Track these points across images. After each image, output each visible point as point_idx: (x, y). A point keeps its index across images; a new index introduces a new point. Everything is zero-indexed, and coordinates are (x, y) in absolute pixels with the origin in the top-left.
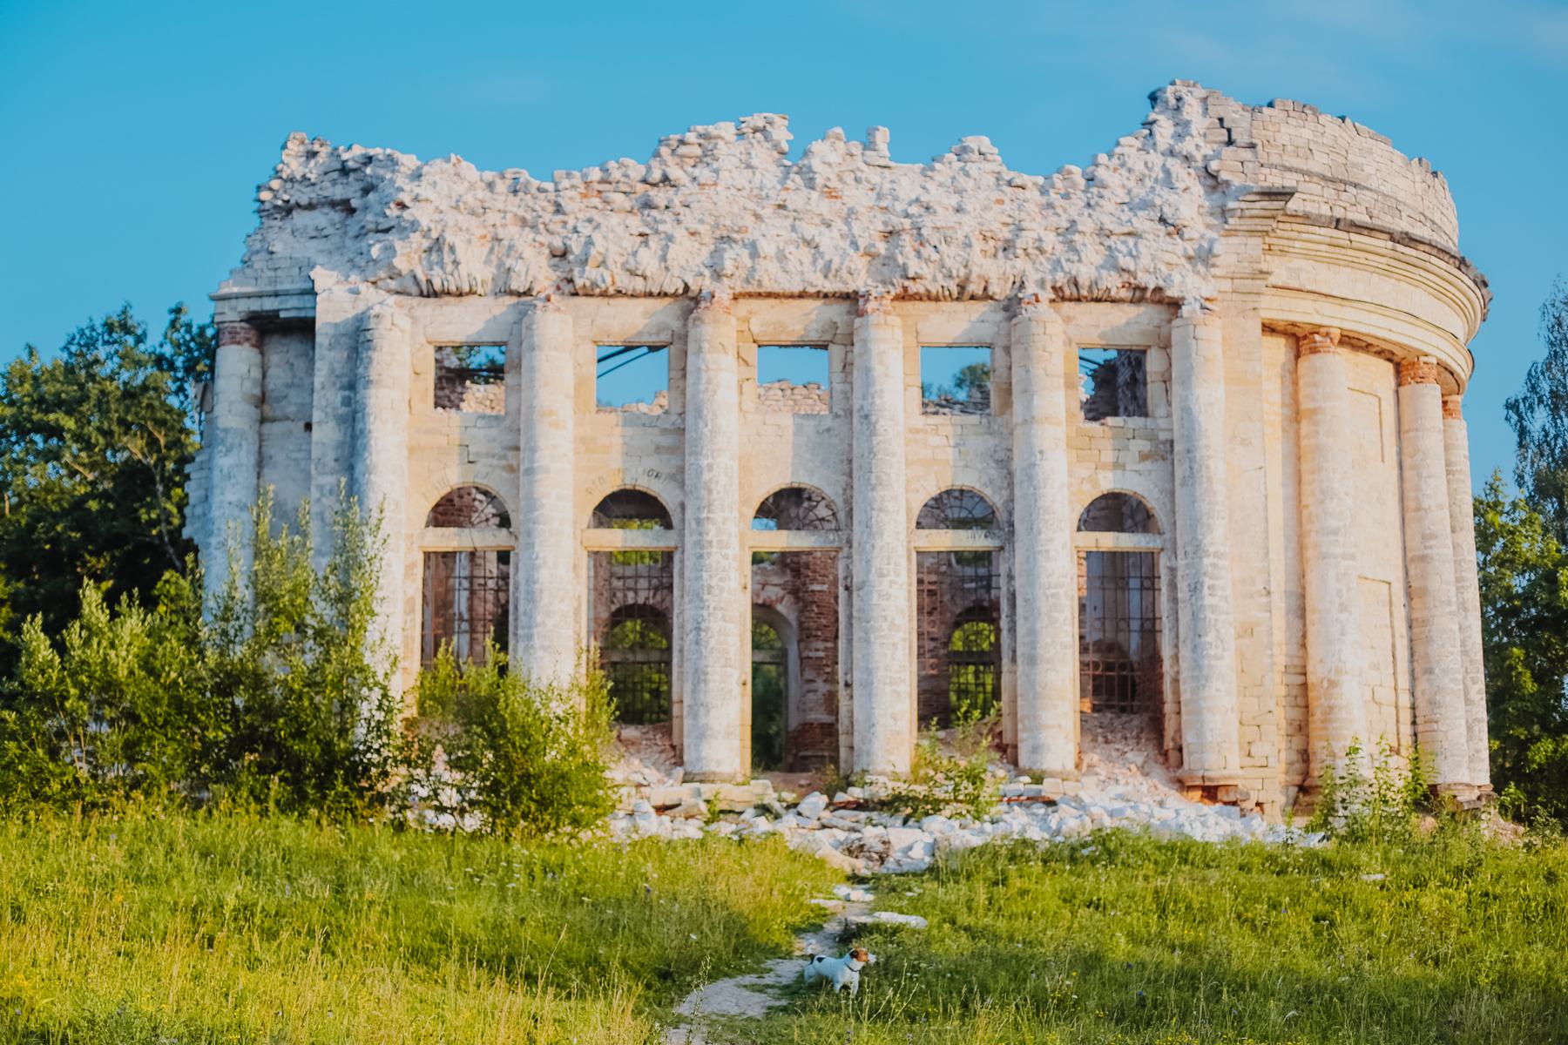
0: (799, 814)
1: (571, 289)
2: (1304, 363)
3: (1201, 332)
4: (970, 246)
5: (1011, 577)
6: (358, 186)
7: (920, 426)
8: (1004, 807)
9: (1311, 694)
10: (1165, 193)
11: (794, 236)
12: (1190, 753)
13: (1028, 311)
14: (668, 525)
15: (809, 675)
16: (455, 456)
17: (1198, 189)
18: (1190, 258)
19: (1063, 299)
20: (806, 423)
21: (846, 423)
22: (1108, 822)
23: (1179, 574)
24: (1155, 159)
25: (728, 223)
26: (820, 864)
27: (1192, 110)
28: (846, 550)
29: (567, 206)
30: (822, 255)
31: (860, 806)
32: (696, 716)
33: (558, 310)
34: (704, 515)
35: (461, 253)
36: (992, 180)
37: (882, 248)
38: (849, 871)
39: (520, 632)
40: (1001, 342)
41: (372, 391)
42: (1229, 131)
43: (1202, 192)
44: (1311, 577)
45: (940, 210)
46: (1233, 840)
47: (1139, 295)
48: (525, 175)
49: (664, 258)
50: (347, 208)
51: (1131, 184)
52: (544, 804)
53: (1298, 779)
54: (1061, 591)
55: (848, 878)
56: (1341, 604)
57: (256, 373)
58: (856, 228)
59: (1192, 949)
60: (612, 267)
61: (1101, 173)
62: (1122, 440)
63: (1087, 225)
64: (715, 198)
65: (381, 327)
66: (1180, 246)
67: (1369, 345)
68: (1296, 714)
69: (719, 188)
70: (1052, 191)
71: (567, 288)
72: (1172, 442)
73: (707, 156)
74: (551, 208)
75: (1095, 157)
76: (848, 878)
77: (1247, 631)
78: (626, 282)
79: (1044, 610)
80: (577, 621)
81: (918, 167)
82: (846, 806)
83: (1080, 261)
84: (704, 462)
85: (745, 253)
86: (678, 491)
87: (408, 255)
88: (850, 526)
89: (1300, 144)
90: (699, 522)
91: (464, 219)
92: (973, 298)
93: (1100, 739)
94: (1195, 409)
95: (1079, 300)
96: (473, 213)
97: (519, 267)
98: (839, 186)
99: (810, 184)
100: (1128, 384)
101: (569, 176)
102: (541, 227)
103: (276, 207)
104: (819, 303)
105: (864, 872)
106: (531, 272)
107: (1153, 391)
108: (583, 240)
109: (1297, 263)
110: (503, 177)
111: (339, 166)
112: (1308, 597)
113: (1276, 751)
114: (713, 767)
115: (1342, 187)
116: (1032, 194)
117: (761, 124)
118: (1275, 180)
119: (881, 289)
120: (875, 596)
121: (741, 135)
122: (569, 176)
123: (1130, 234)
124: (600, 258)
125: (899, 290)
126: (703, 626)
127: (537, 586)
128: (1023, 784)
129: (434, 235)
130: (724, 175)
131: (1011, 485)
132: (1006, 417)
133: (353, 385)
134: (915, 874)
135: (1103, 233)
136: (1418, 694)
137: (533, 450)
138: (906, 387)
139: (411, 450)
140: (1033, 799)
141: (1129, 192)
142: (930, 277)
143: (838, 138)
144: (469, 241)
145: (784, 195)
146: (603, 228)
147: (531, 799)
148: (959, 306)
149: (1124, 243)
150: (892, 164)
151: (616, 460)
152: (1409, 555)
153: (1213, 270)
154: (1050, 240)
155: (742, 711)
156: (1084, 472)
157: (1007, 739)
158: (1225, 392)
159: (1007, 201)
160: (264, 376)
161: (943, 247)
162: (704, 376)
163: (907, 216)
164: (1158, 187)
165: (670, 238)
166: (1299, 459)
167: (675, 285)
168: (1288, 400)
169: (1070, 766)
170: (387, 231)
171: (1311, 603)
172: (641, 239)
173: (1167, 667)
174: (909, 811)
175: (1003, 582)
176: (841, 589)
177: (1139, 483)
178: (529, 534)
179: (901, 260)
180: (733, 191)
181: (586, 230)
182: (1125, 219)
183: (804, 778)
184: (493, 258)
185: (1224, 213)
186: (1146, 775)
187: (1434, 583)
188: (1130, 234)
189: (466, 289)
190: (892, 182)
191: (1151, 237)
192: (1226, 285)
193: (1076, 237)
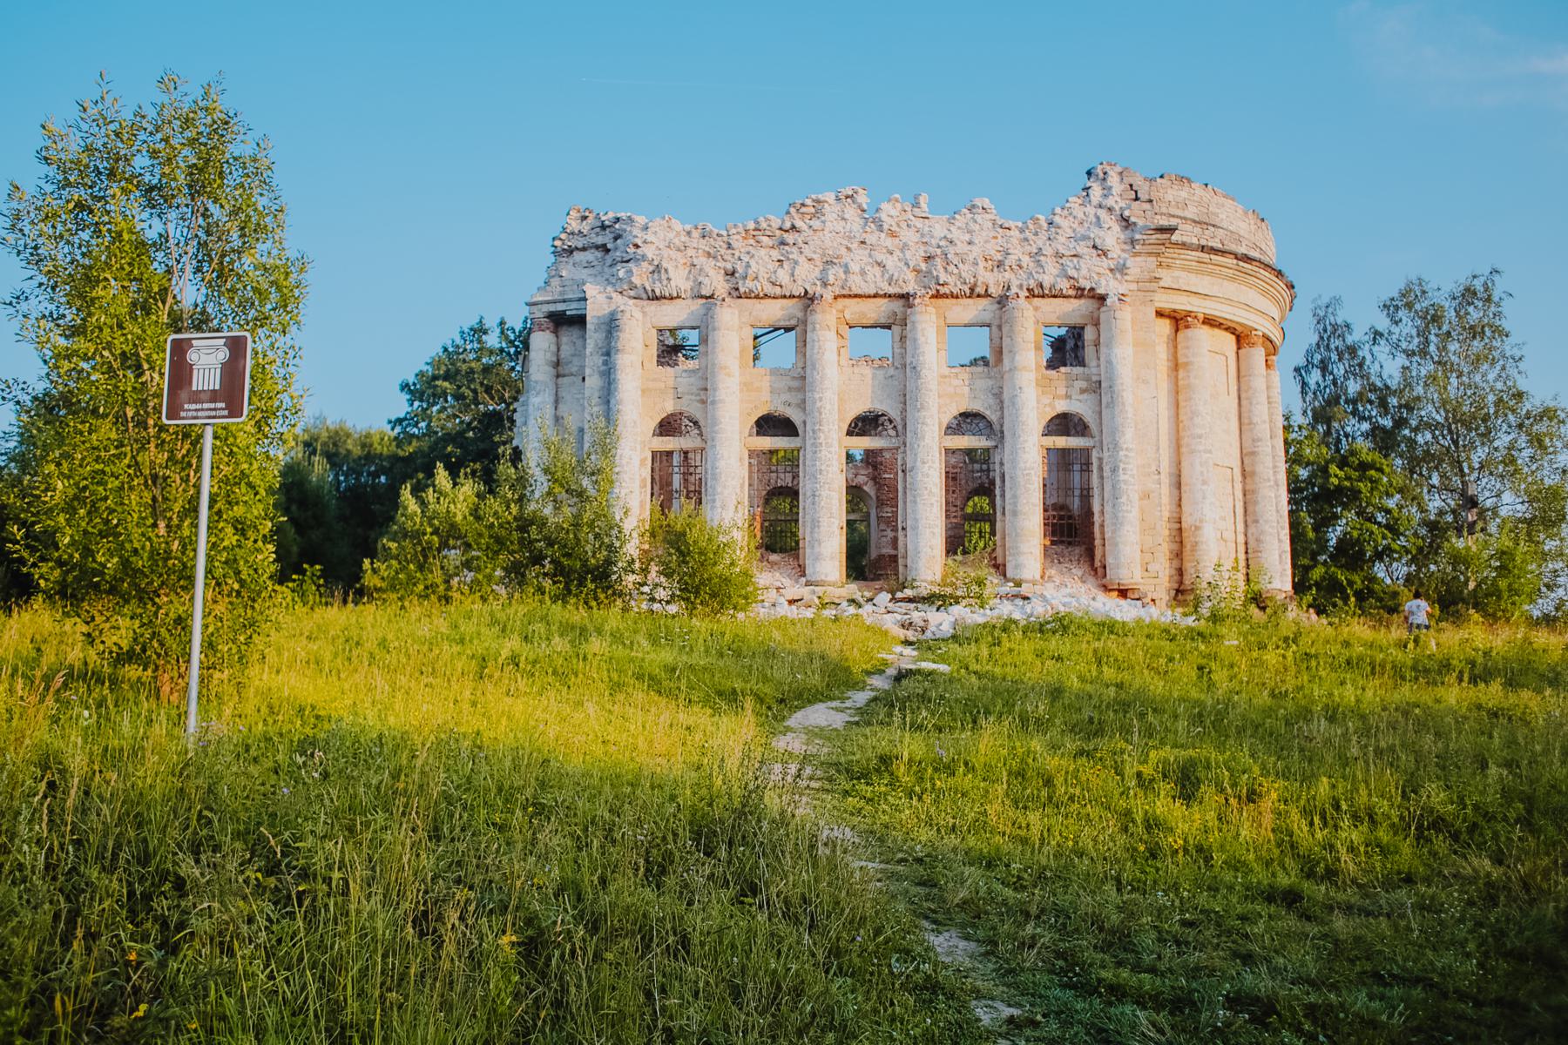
5: (1002, 464)
10: (1096, 230)
13: (1012, 304)
17: (1116, 228)
21: (902, 371)
24: (1090, 210)
27: (1113, 180)
31: (910, 600)
35: (671, 275)
37: (923, 266)
40: (996, 322)
47: (1080, 293)
50: (605, 249)
53: (1176, 586)
57: (554, 348)
58: (908, 254)
59: (1120, 686)
61: (1057, 219)
62: (1071, 379)
63: (1048, 251)
66: (1105, 263)
68: (1175, 547)
71: (735, 294)
77: (1146, 496)
84: (817, 396)
88: (905, 434)
89: (1177, 201)
91: (673, 253)
97: (706, 281)
105: (912, 639)
107: (1089, 351)
109: (1177, 273)
116: (1015, 233)
121: (838, 199)
131: (1002, 408)
133: (608, 353)
137: (715, 390)
139: (643, 391)
148: (970, 301)
151: (766, 396)
154: (1026, 260)
156: (1046, 400)
158: (1132, 349)
173: (1097, 518)
177: (1079, 406)
181: (746, 258)
183: (877, 584)
185: (1133, 242)
187: (1259, 468)
192: (1134, 286)
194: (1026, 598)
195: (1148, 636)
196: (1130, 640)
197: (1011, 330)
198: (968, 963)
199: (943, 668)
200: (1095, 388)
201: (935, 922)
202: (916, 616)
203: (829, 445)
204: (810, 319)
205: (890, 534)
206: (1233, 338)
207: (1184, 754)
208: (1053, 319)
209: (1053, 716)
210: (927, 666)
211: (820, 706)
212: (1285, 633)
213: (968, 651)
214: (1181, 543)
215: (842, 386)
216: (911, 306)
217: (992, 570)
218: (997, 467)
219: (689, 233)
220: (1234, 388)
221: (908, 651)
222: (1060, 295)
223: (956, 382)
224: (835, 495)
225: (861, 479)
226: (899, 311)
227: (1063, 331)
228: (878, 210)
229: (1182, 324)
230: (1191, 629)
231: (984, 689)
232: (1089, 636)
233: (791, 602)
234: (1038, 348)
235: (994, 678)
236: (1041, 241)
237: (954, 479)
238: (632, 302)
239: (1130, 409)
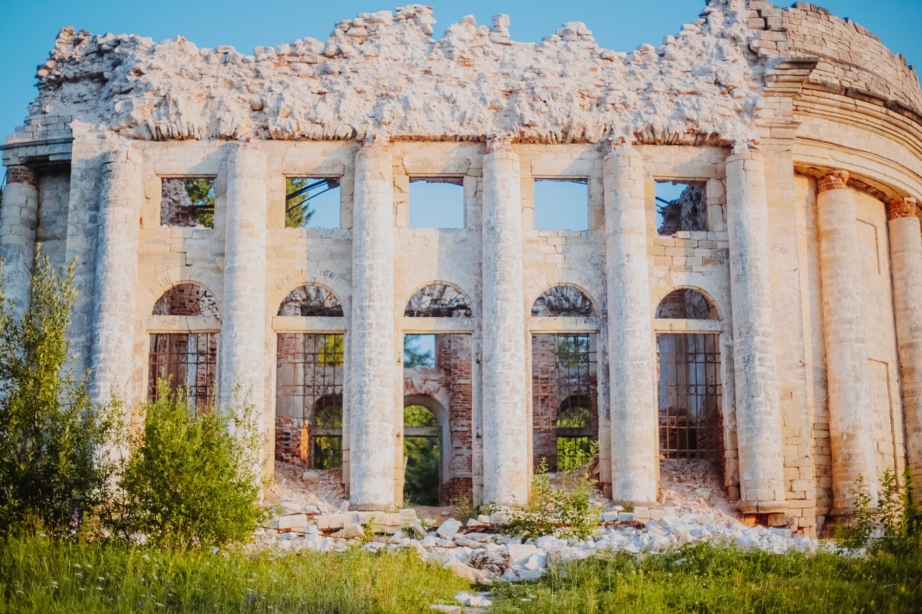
0: (438, 536)
1: (268, 135)
2: (822, 197)
4: (571, 101)
5: (605, 353)
6: (109, 63)
7: (534, 238)
8: (603, 530)
9: (834, 446)
10: (719, 63)
11: (437, 94)
12: (747, 489)
15: (457, 443)
16: (178, 260)
17: (743, 61)
18: (738, 112)
19: (643, 143)
20: (446, 235)
21: (477, 239)
22: (690, 538)
23: (735, 350)
24: (711, 40)
25: (386, 84)
26: (449, 573)
28: (477, 332)
29: (264, 72)
30: (458, 108)
31: (487, 529)
32: (359, 460)
33: (256, 148)
34: (366, 304)
35: (182, 107)
36: (587, 54)
38: (473, 580)
39: (222, 394)
40: (595, 175)
41: (110, 209)
42: (765, 19)
43: (746, 64)
44: (832, 357)
45: (548, 75)
46: (792, 551)
47: (701, 139)
48: (232, 51)
49: (337, 110)
50: (100, 79)
51: (693, 58)
52: (193, 516)
53: (824, 510)
54: (645, 363)
55: (472, 587)
56: (855, 376)
57: (32, 204)
58: (485, 88)
60: (298, 117)
61: (670, 50)
63: (659, 86)
64: (377, 66)
65: (118, 160)
66: (731, 103)
67: (869, 187)
68: (822, 460)
69: (379, 59)
70: (633, 63)
71: (264, 134)
72: (727, 250)
73: (371, 36)
74: (252, 74)
75: (665, 38)
76: (472, 587)
78: (308, 128)
79: (632, 377)
80: (267, 387)
81: (531, 44)
82: (475, 530)
83: (655, 113)
84: (366, 263)
85: (399, 107)
86: (347, 287)
87: (142, 108)
88: (480, 314)
90: (362, 309)
91: (185, 82)
92: (573, 141)
93: (675, 479)
94: (746, 223)
95: (654, 144)
96: (193, 78)
97: (227, 117)
98: (471, 57)
99: (449, 55)
100: (689, 215)
101: (266, 50)
102: (244, 88)
103: (50, 81)
104: (457, 144)
105: (486, 581)
106: (235, 121)
107: (713, 212)
108: (275, 97)
109: (817, 121)
110: (216, 52)
111: (96, 49)
112: (829, 372)
114: (372, 501)
115: (847, 67)
116: (618, 65)
117: (412, 11)
119: (504, 133)
120: (500, 366)
121: (397, 20)
122: (266, 50)
123: (693, 93)
124: (288, 110)
125: (518, 135)
126: (365, 389)
127: (235, 359)
128: (616, 513)
129: (162, 93)
130: (383, 49)
131: (605, 282)
132: (599, 231)
134: (530, 583)
135: (673, 92)
136: (910, 446)
137: (234, 254)
138: (523, 208)
139: (141, 256)
140: (627, 523)
141: (691, 64)
142: (541, 125)
143: (471, 22)
144: (189, 98)
145: (429, 64)
146: (291, 88)
147: (180, 512)
148: (563, 147)
149: (688, 99)
150: (511, 42)
151: (301, 263)
152: (900, 343)
153: (757, 121)
154: (632, 98)
155: (396, 457)
156: (661, 272)
157: (603, 478)
158: (765, 210)
159: (599, 69)
160: (39, 206)
161: (551, 102)
162: (366, 197)
163: (523, 79)
164: (713, 60)
165: (342, 95)
166: (820, 268)
168: (811, 225)
169: (653, 499)
170: (127, 92)
172: (319, 96)
173: (727, 422)
174: (526, 533)
175: (599, 357)
176: (474, 363)
177: (703, 281)
178: (230, 319)
179: (518, 111)
180: (391, 61)
181: (278, 89)
182: (689, 81)
183: (445, 510)
184: (208, 111)
185: (763, 78)
186: (713, 505)
188: (693, 93)
189: (186, 134)
190: (512, 54)
191: (709, 95)
192: (766, 132)
193: (652, 95)
200: (722, 257)
202: (493, 550)
206: (880, 206)
214: (830, 459)
219: (207, 58)
229: (822, 184)
236: (651, 74)
238: (130, 142)
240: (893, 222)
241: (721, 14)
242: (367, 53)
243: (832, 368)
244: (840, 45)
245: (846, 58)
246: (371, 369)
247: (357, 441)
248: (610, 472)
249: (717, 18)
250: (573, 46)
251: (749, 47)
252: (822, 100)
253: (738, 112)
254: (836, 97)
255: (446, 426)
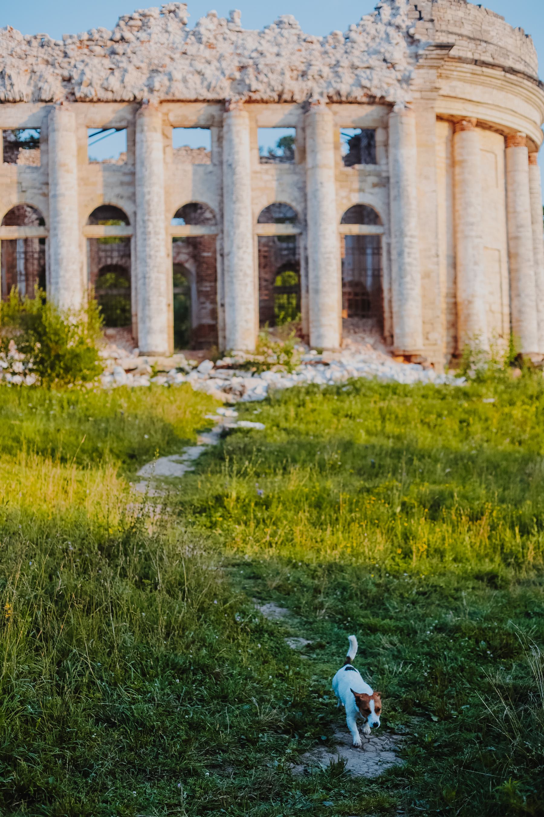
1: (73, 98)
3: (405, 120)
5: (306, 249)
9: (460, 307)
13: (314, 109)
14: (128, 223)
17: (403, 44)
21: (219, 165)
24: (381, 27)
30: (206, 79)
31: (229, 367)
32: (144, 322)
33: (67, 109)
35: (14, 80)
36: (295, 38)
37: (238, 75)
38: (224, 401)
40: (300, 125)
42: (420, 12)
45: (268, 55)
47: (372, 100)
49: (122, 81)
53: (451, 351)
58: (224, 64)
59: (398, 438)
61: (353, 35)
62: (363, 175)
63: (345, 63)
66: (395, 75)
68: (451, 318)
71: (72, 98)
74: (62, 55)
77: (427, 275)
80: (82, 274)
84: (146, 190)
88: (222, 222)
90: (144, 222)
91: (15, 61)
92: (286, 101)
96: (20, 58)
97: (46, 87)
99: (200, 41)
102: (57, 65)
105: (232, 401)
107: (379, 151)
108: (79, 72)
109: (454, 83)
113: (441, 337)
116: (316, 46)
117: (173, 8)
118: (444, 39)
119: (238, 97)
121: (162, 13)
123: (368, 68)
124: (89, 82)
130: (154, 36)
131: (306, 201)
135: (354, 67)
136: (513, 306)
137: (56, 185)
140: (318, 363)
141: (367, 45)
144: (19, 73)
145: (186, 47)
146: (90, 65)
150: (243, 30)
151: (100, 190)
154: (326, 71)
156: (343, 193)
158: (416, 150)
161: (270, 75)
163: (251, 58)
167: (129, 96)
171: (460, 261)
173: (386, 294)
177: (372, 199)
179: (247, 82)
180: (159, 45)
181: (81, 66)
182: (365, 59)
183: (200, 354)
185: (417, 56)
188: (368, 68)
190: (243, 40)
191: (378, 69)
192: (418, 95)
194: (326, 364)
195: (423, 396)
196: (409, 401)
197: (314, 133)
198: (282, 619)
199: (258, 426)
200: (384, 182)
201: (260, 598)
202: (235, 382)
203: (157, 233)
204: (139, 122)
205: (209, 306)
206: (501, 139)
207: (437, 488)
208: (348, 122)
209: (344, 463)
210: (245, 424)
211: (164, 460)
212: (530, 392)
213: (277, 412)
214: (456, 315)
215: (167, 183)
216: (227, 110)
217: (299, 340)
218: (302, 251)
219: (29, 43)
220: (502, 182)
221: (230, 413)
222: (355, 102)
223: (267, 177)
224: (163, 277)
225: (183, 257)
226: (217, 115)
227: (358, 132)
228: (198, 24)
229: (458, 127)
230: (458, 390)
231: (291, 443)
232: (377, 397)
233: (128, 371)
234: (337, 147)
235: (299, 433)
236: (339, 54)
237: (265, 257)
239: (414, 203)
240: (509, 150)
241: (390, 8)
242: (142, 39)
243: (460, 255)
244: (474, 26)
245: (478, 36)
246: (151, 263)
247: (143, 309)
248: (308, 328)
249: (386, 11)
250: (285, 32)
251: (408, 32)
252: (459, 69)
253: (399, 81)
254: (469, 66)
255: (194, 287)
